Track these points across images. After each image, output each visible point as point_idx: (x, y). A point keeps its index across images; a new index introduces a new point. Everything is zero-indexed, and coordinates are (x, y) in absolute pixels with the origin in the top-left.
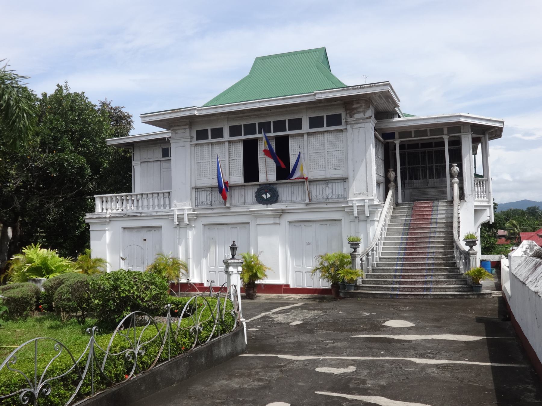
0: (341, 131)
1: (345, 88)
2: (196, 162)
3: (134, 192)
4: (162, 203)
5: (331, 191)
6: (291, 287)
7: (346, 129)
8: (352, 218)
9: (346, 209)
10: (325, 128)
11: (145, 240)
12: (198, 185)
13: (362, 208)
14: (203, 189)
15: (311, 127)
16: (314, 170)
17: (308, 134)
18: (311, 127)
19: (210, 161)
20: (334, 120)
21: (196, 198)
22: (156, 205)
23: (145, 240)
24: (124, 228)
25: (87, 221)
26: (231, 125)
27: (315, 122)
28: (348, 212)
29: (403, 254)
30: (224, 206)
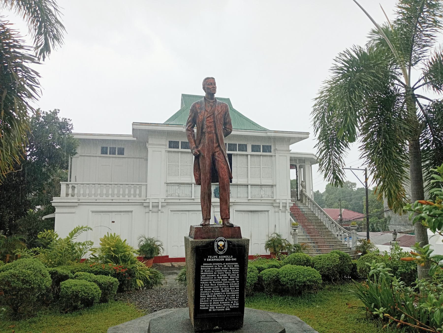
0: (271, 156)
1: (265, 130)
2: (168, 164)
3: (70, 181)
4: (132, 192)
5: (264, 193)
6: (170, 257)
7: (275, 156)
8: (147, 210)
9: (144, 204)
10: (261, 153)
11: (113, 222)
12: (168, 182)
13: (158, 204)
14: (173, 185)
15: (253, 151)
16: (173, 176)
17: (251, 155)
18: (253, 151)
19: (180, 164)
20: (267, 149)
21: (167, 191)
22: (131, 194)
23: (113, 222)
24: (93, 212)
25: (53, 204)
26: (183, 141)
27: (255, 148)
28: (145, 206)
29: (327, 236)
30: (190, 198)
